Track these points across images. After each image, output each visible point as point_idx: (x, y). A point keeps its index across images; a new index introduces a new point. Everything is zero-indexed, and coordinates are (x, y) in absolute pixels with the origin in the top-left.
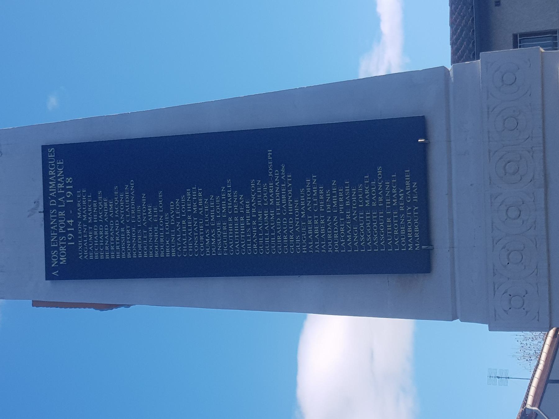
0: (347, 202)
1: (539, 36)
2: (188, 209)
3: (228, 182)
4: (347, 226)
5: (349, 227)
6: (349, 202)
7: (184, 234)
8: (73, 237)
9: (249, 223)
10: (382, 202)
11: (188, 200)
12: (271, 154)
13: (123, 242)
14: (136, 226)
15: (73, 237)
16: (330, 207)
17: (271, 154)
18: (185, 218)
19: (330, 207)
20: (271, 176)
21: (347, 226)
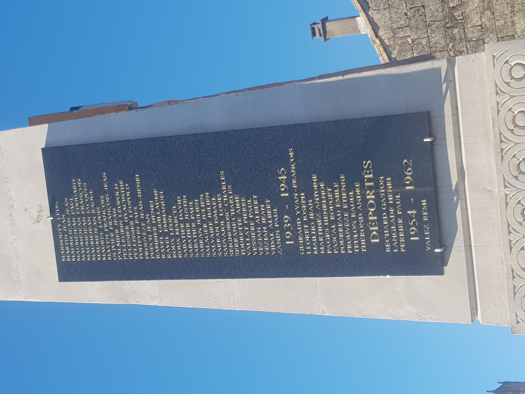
0: (195, 245)
1: (340, 78)
2: (153, 220)
3: (365, 167)
4: (259, 242)
5: (260, 244)
6: (197, 245)
7: (207, 246)
8: (417, 231)
9: (351, 251)
10: (351, 249)
11: (342, 190)
12: (304, 197)
13: (129, 240)
14: (169, 235)
15: (417, 231)
16: (230, 245)
17: (304, 197)
18: (112, 231)
19: (230, 245)
20: (107, 190)
21: (259, 242)
